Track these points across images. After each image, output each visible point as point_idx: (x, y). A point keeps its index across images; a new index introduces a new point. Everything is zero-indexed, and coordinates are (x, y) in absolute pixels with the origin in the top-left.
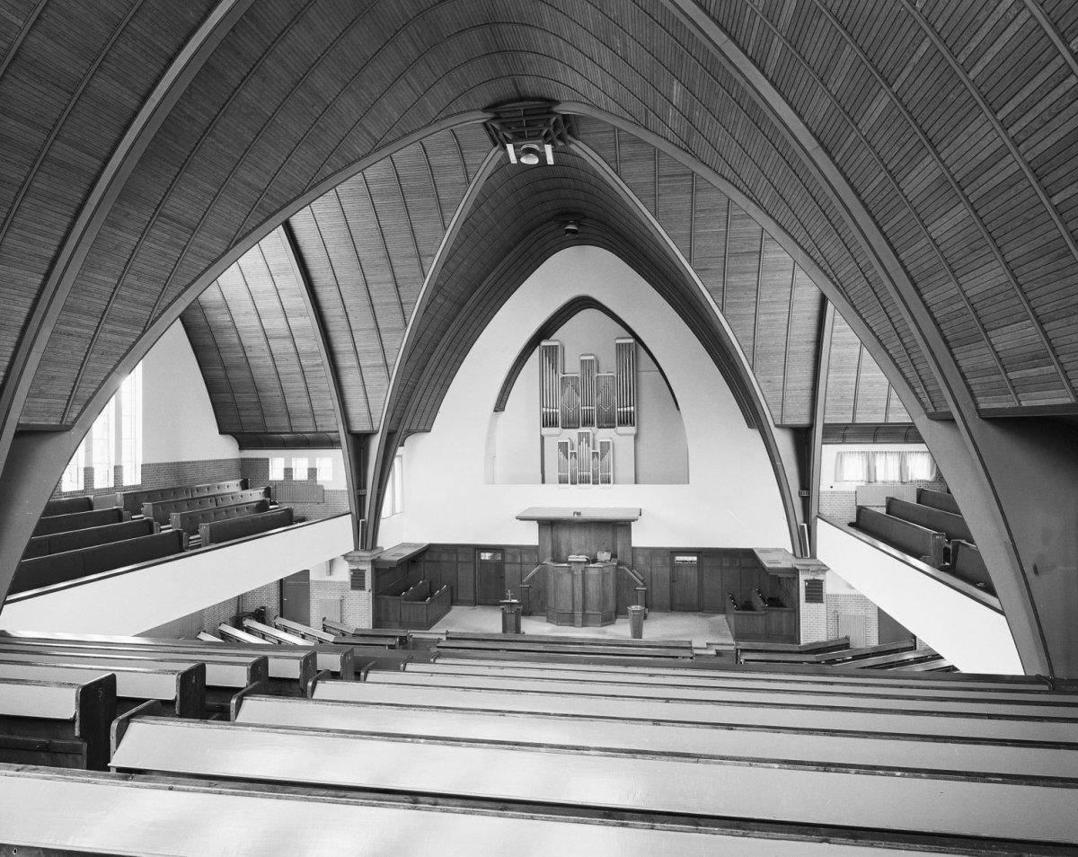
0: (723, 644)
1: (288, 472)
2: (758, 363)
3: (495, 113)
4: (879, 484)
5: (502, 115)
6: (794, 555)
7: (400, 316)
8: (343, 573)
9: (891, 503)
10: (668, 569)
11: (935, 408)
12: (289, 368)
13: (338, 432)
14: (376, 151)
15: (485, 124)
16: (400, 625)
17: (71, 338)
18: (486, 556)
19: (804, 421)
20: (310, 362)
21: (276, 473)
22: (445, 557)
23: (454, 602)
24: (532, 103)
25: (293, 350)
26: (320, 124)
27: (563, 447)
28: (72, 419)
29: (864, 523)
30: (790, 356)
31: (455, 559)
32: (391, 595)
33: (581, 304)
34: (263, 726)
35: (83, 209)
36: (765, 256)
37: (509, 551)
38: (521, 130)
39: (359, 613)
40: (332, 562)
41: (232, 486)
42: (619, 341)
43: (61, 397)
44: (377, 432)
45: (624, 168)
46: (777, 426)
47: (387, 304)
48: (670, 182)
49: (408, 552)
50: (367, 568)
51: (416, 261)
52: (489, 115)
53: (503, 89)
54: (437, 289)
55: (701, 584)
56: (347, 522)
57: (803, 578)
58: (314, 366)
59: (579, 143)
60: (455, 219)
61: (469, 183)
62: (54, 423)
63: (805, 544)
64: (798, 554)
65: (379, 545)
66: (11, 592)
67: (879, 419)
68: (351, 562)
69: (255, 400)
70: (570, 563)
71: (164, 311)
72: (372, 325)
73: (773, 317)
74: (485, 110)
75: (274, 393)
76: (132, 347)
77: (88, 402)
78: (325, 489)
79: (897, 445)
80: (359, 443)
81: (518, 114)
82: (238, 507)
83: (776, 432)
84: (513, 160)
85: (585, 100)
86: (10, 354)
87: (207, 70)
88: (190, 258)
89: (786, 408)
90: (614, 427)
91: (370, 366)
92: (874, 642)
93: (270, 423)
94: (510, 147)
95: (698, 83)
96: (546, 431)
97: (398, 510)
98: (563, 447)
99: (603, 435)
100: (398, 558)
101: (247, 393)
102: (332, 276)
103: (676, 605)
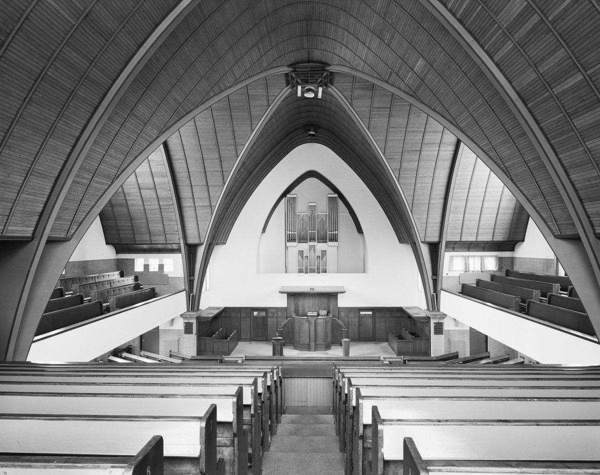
0: (391, 358)
1: (146, 267)
2: (414, 209)
3: (294, 68)
4: (470, 272)
5: (297, 70)
6: (428, 309)
7: (221, 179)
8: (180, 325)
9: (479, 282)
10: (357, 319)
11: (560, 233)
12: (152, 206)
13: (179, 244)
14: (236, 85)
15: (287, 75)
16: (213, 353)
17: (78, 185)
18: (255, 313)
19: (436, 239)
20: (165, 203)
21: (139, 267)
22: (233, 315)
23: (239, 338)
24: (314, 64)
25: (155, 196)
26: (215, 68)
27: (301, 253)
28: (71, 234)
29: (466, 291)
30: (431, 206)
31: (239, 316)
32: (208, 337)
33: (311, 174)
34: (442, 397)
35: (97, 109)
36: (423, 153)
37: (269, 310)
38: (306, 78)
39: (189, 346)
40: (172, 320)
41: (115, 276)
42: (329, 196)
43: (68, 220)
44: (203, 244)
45: (355, 103)
46: (422, 242)
47: (214, 171)
48: (378, 111)
49: (216, 312)
50: (194, 321)
51: (233, 148)
52: (291, 69)
53: (303, 55)
54: (243, 164)
55: (374, 328)
56: (183, 295)
57: (432, 322)
58: (168, 205)
59: (333, 87)
60: (259, 126)
61: (269, 106)
62: (63, 236)
63: (434, 304)
64: (431, 309)
65: (200, 308)
66: (37, 335)
67: (473, 239)
68: (184, 318)
69: (130, 224)
70: (308, 316)
71: (123, 171)
72: (204, 183)
73: (424, 185)
74: (289, 66)
75: (142, 221)
76: (105, 192)
77: (81, 223)
78: (169, 276)
79: (464, 252)
80: (191, 250)
81: (307, 70)
82: (119, 288)
83: (421, 245)
84: (299, 94)
85: (348, 65)
86: (48, 194)
87: (173, 35)
88: (140, 140)
89: (427, 232)
90: (307, 242)
91: (201, 206)
92: (468, 354)
93: (138, 238)
94: (299, 88)
95: (437, 62)
96: (289, 244)
97: (208, 289)
98: (301, 253)
99: (320, 246)
100: (211, 315)
101: (125, 220)
102: (183, 154)
103: (361, 338)
